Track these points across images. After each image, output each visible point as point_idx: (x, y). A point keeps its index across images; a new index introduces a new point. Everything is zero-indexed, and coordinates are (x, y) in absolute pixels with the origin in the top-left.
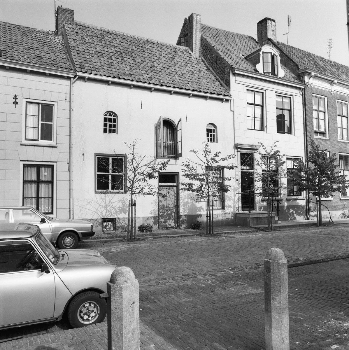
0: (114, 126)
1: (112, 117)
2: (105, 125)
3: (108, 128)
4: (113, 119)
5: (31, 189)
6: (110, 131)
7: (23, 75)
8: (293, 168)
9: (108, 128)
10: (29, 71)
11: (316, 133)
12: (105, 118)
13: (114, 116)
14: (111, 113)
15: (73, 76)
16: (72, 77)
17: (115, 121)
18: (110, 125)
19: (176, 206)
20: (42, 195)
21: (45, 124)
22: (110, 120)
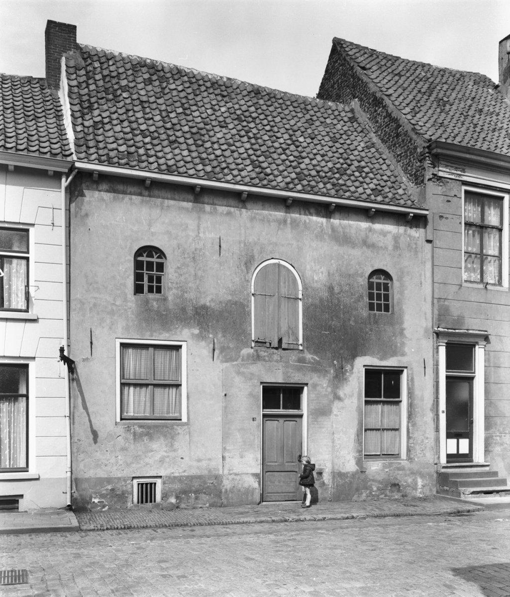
0: (159, 280)
1: (155, 260)
2: (138, 277)
3: (146, 282)
4: (157, 263)
5: (135, 369)
6: (151, 290)
7: (8, 186)
8: (509, 493)
9: (146, 282)
10: (52, 173)
11: (466, 281)
12: (370, 304)
13: (158, 258)
14: (149, 250)
15: (66, 170)
16: (65, 173)
17: (160, 267)
18: (151, 279)
19: (383, 528)
20: (174, 393)
21: (251, 310)
22: (150, 265)
